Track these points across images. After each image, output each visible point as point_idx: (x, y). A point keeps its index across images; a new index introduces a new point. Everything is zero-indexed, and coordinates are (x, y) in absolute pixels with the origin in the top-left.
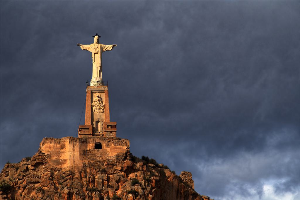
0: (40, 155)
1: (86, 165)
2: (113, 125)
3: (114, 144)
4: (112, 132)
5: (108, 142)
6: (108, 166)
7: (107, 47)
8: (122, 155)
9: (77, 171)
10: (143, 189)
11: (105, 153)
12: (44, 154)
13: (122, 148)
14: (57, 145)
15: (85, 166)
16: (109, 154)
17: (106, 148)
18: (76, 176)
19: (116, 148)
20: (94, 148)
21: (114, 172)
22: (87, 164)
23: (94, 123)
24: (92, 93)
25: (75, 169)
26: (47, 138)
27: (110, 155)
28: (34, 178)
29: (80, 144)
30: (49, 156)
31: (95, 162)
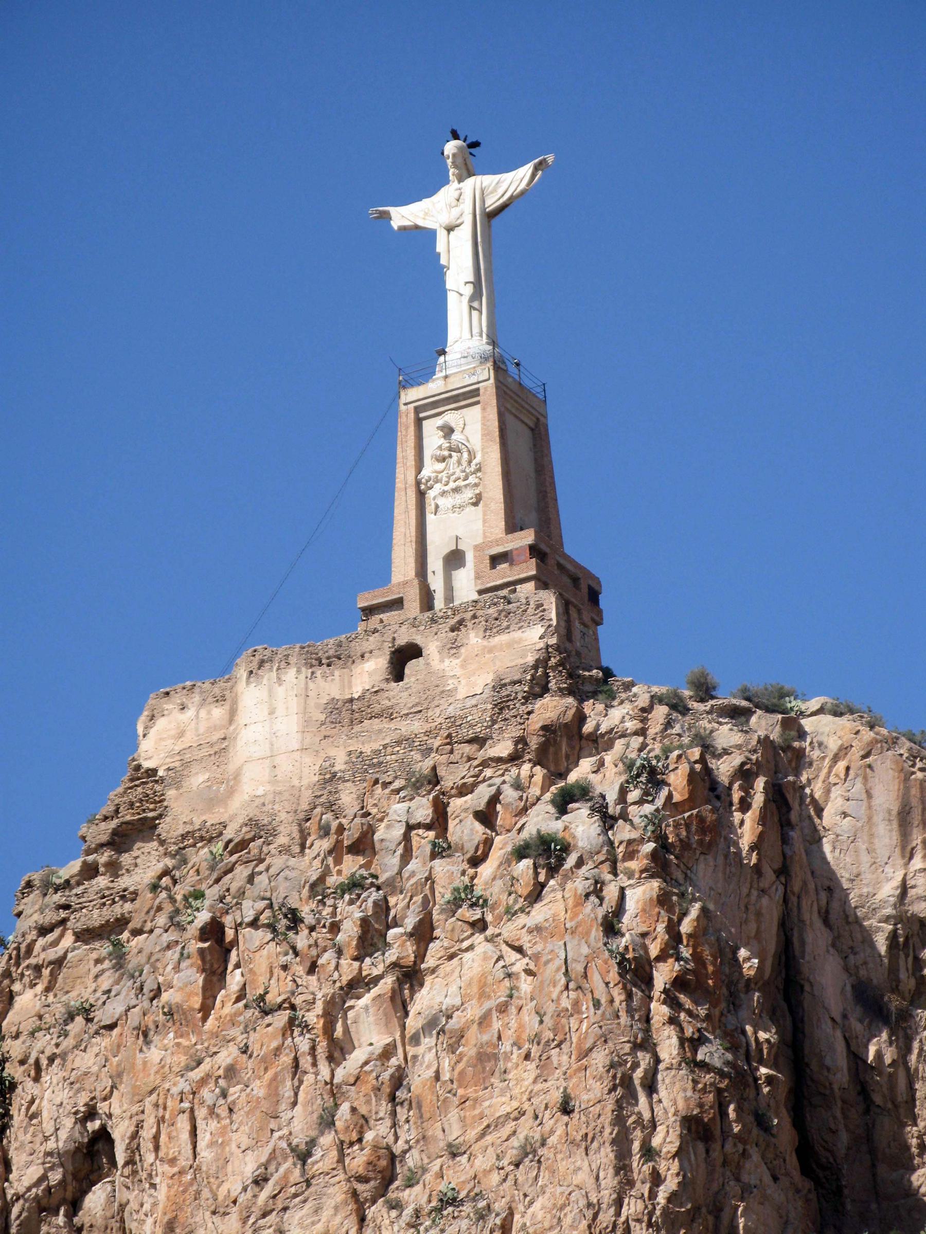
0: (137, 782)
1: (334, 775)
2: (517, 549)
3: (481, 634)
4: (518, 587)
5: (453, 630)
6: (451, 752)
7: (508, 182)
8: (516, 678)
9: (283, 816)
10: (608, 821)
11: (438, 690)
12: (154, 771)
13: (520, 640)
14: (209, 713)
15: (330, 779)
16: (456, 689)
17: (442, 661)
18: (282, 840)
19: (490, 651)
20: (387, 680)
21: (477, 776)
22: (339, 766)
23: (435, 564)
24: (419, 422)
25: (276, 807)
26: (168, 690)
27: (462, 693)
28: (104, 904)
29: (308, 672)
30: (177, 777)
31: (385, 747)
